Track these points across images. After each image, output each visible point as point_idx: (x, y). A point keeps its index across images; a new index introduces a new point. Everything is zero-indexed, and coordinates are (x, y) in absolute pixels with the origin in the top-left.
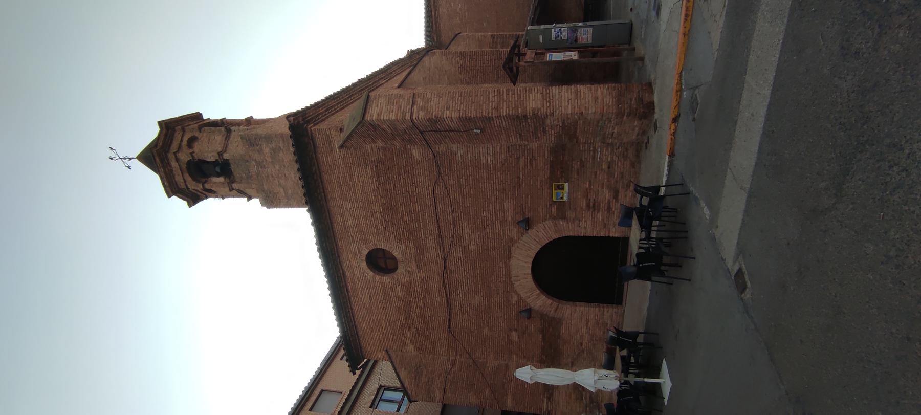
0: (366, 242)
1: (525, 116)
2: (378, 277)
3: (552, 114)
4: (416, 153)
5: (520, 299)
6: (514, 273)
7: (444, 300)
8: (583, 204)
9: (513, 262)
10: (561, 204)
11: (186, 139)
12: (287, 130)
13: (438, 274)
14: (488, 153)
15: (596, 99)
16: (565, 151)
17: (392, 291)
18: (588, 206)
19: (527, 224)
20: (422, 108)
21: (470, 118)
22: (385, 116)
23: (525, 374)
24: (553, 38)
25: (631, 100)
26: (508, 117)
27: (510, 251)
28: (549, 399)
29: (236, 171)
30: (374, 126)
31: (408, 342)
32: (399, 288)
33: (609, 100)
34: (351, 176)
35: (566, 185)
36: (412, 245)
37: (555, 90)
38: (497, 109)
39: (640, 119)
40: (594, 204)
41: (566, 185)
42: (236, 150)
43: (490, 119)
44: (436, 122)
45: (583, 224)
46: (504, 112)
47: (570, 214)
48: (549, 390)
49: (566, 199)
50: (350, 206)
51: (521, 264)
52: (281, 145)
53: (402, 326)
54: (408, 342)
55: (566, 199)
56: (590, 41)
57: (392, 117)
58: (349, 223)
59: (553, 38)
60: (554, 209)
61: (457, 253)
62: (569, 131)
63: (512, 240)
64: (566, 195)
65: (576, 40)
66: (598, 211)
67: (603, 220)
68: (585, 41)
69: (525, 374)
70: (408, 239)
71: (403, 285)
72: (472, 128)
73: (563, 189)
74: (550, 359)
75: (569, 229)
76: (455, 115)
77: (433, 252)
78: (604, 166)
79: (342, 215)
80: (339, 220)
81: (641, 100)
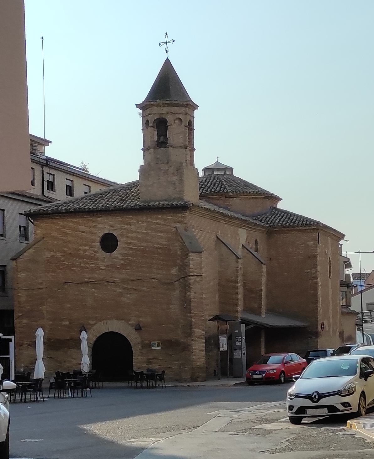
0: (122, 234)
1: (191, 329)
2: (99, 239)
3: (192, 340)
4: (174, 271)
5: (92, 325)
6: (109, 322)
7: (87, 280)
8: (151, 357)
9: (115, 321)
10: (150, 346)
11: (180, 116)
12: (209, 162)
13: (104, 278)
14: (175, 309)
15: (199, 358)
16: (176, 347)
17: (90, 248)
18: (150, 359)
19: (138, 328)
20: (195, 280)
21: (191, 304)
22: (191, 262)
23: (40, 333)
24: (237, 338)
25: (199, 373)
26: (191, 321)
27: (122, 320)
28: (29, 345)
29: (161, 150)
30: (187, 255)
31: (52, 254)
32: (92, 252)
33: (198, 364)
34: (161, 232)
35: (160, 348)
36: (122, 263)
37: (204, 341)
38: (195, 316)
39: (191, 377)
40: (151, 362)
41: (160, 348)
42: (175, 154)
43: (190, 313)
44: (189, 287)
45: (140, 357)
46: (193, 319)
47: (145, 351)
48: (33, 345)
49: (153, 348)
50: (144, 228)
51: (115, 326)
52: (177, 189)
53: (64, 252)
54: (52, 254)
55: (153, 348)
56: (235, 357)
57: (191, 266)
58: (133, 226)
59: (237, 338)
60: (146, 342)
61: (119, 290)
62: (186, 348)
63: (129, 320)
64: (155, 348)
65: (235, 350)
66: (147, 364)
67: (143, 367)
68: (235, 354)
69: (40, 333)
70: (125, 262)
71: (95, 255)
72: (186, 303)
73: (158, 346)
74: (50, 344)
75: (136, 350)
76: (192, 297)
77: (118, 276)
78: (170, 366)
79: (138, 222)
80: (134, 220)
81: (198, 377)
